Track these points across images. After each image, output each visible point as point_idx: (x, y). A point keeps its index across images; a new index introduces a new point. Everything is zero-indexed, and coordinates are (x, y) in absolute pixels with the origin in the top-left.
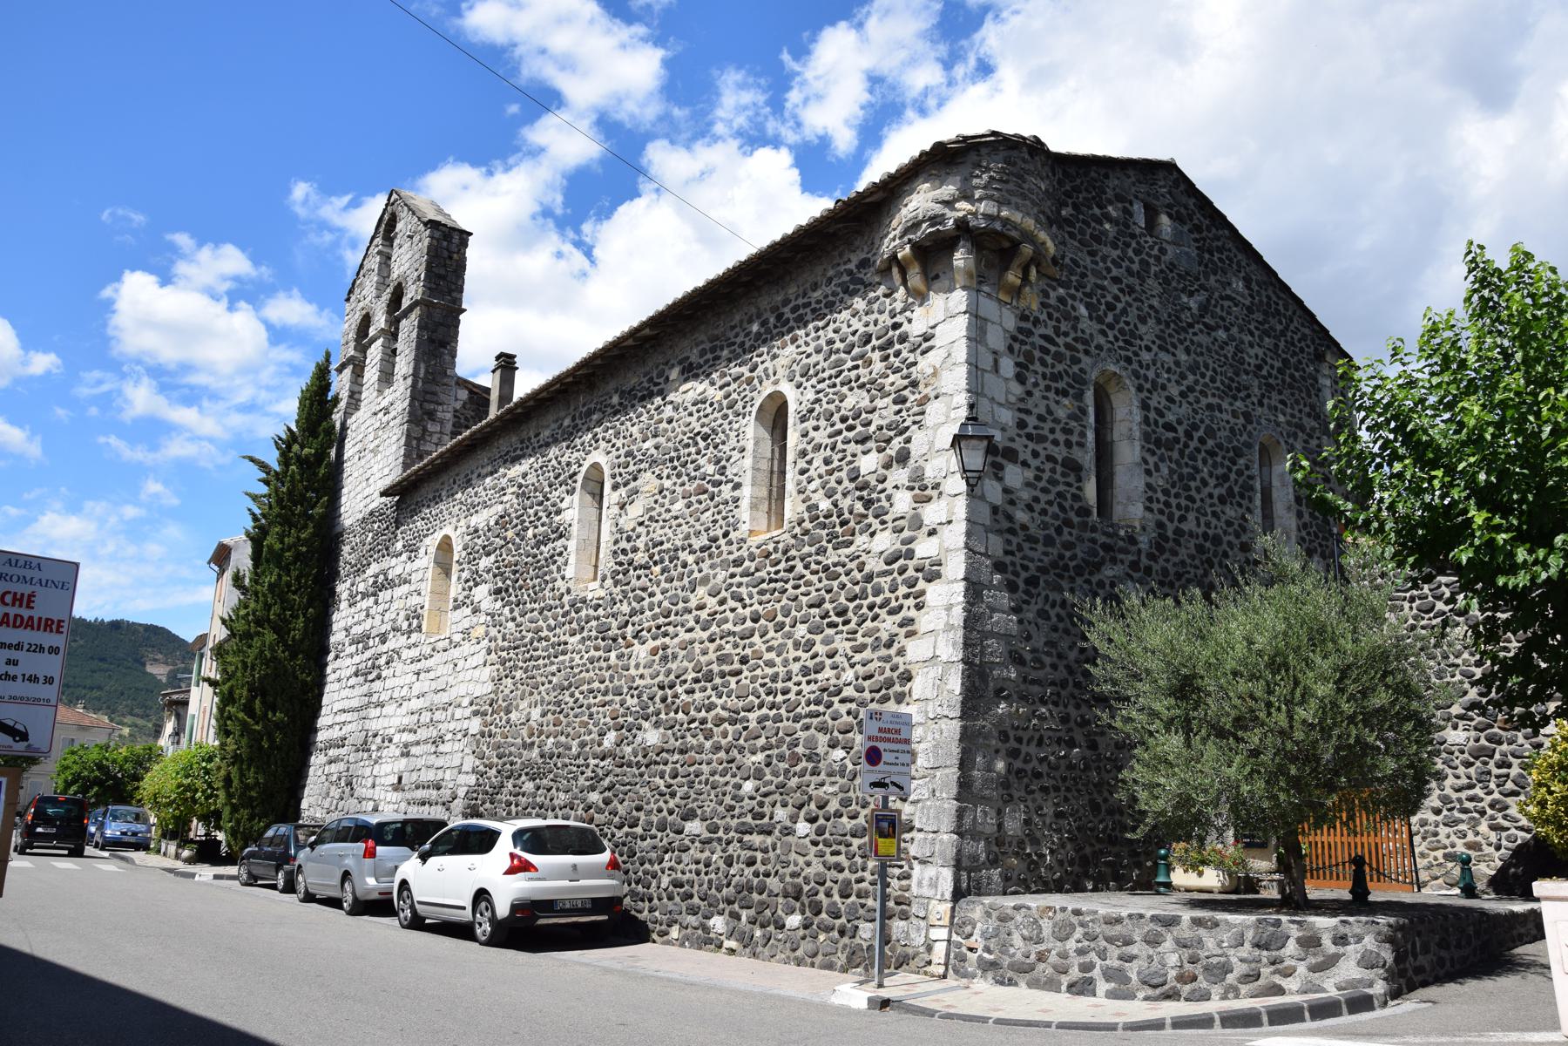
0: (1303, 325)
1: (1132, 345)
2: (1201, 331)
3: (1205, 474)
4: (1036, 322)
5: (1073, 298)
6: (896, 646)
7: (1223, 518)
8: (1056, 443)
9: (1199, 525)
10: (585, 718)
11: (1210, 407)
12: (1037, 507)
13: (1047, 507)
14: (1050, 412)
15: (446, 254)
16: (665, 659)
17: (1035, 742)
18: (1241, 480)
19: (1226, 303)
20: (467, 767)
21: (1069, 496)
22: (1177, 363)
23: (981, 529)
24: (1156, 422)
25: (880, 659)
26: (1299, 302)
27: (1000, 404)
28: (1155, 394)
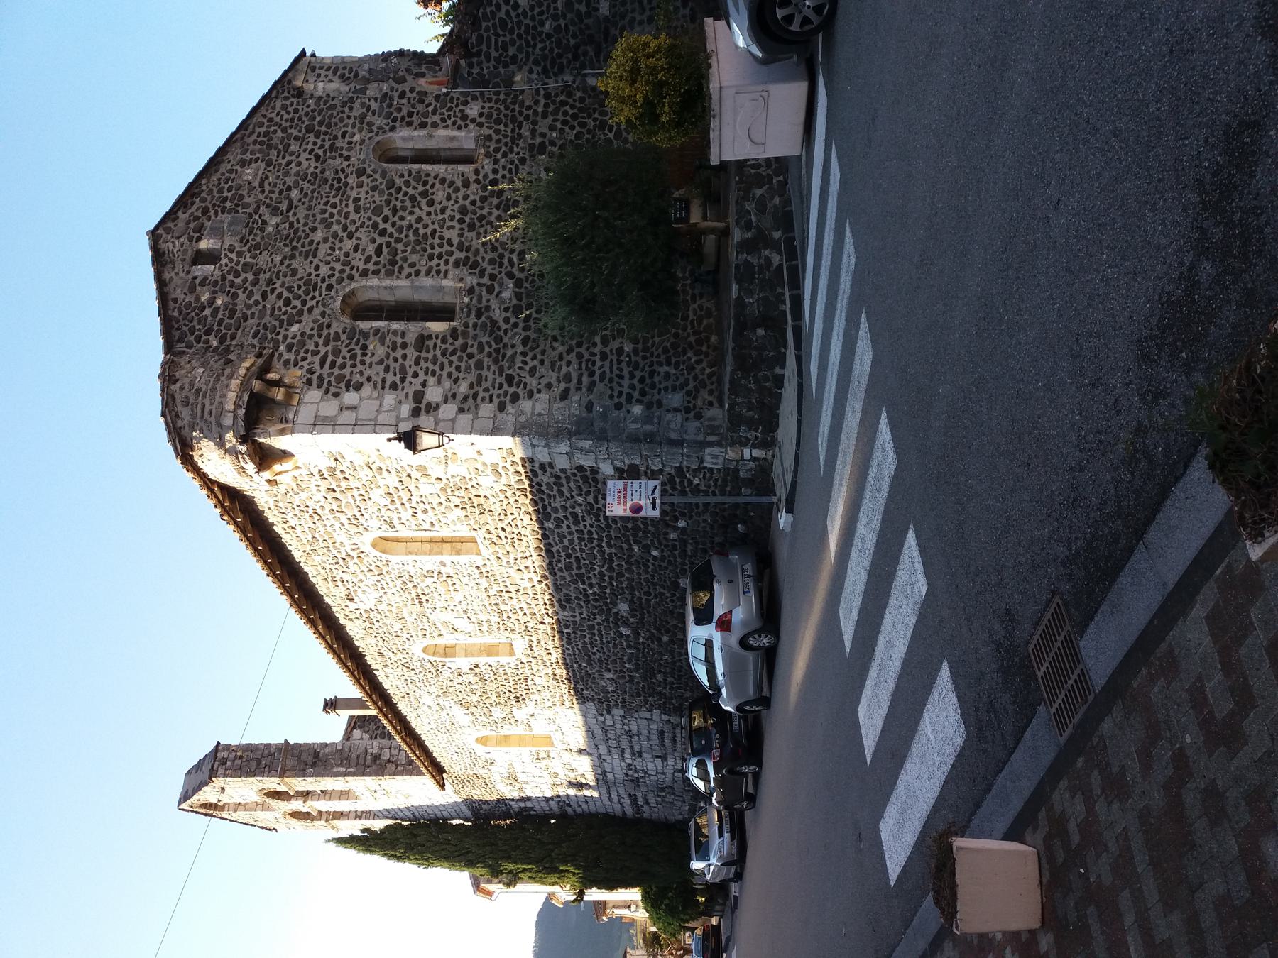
0: (274, 108)
1: (316, 284)
2: (295, 214)
3: (412, 218)
4: (311, 371)
5: (285, 337)
6: (559, 474)
7: (445, 203)
8: (404, 357)
9: (453, 227)
10: (611, 645)
11: (357, 210)
12: (455, 375)
13: (454, 366)
14: (381, 362)
15: (238, 762)
16: (568, 601)
17: (620, 381)
18: (413, 183)
19: (267, 188)
20: (648, 716)
21: (444, 346)
22: (326, 240)
23: (475, 421)
24: (376, 263)
25: (568, 483)
26: (254, 110)
27: (381, 405)
28: (353, 263)
